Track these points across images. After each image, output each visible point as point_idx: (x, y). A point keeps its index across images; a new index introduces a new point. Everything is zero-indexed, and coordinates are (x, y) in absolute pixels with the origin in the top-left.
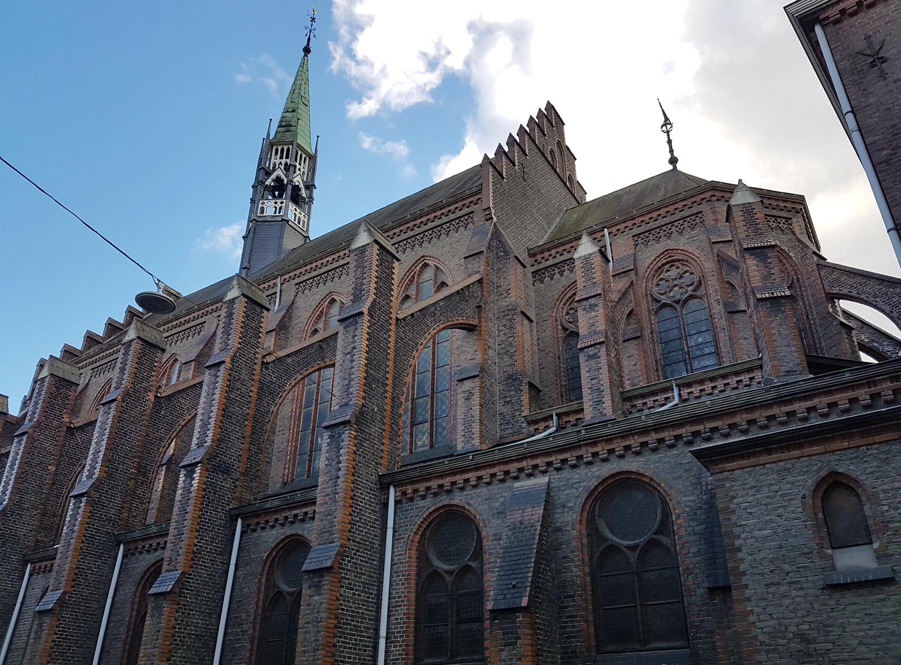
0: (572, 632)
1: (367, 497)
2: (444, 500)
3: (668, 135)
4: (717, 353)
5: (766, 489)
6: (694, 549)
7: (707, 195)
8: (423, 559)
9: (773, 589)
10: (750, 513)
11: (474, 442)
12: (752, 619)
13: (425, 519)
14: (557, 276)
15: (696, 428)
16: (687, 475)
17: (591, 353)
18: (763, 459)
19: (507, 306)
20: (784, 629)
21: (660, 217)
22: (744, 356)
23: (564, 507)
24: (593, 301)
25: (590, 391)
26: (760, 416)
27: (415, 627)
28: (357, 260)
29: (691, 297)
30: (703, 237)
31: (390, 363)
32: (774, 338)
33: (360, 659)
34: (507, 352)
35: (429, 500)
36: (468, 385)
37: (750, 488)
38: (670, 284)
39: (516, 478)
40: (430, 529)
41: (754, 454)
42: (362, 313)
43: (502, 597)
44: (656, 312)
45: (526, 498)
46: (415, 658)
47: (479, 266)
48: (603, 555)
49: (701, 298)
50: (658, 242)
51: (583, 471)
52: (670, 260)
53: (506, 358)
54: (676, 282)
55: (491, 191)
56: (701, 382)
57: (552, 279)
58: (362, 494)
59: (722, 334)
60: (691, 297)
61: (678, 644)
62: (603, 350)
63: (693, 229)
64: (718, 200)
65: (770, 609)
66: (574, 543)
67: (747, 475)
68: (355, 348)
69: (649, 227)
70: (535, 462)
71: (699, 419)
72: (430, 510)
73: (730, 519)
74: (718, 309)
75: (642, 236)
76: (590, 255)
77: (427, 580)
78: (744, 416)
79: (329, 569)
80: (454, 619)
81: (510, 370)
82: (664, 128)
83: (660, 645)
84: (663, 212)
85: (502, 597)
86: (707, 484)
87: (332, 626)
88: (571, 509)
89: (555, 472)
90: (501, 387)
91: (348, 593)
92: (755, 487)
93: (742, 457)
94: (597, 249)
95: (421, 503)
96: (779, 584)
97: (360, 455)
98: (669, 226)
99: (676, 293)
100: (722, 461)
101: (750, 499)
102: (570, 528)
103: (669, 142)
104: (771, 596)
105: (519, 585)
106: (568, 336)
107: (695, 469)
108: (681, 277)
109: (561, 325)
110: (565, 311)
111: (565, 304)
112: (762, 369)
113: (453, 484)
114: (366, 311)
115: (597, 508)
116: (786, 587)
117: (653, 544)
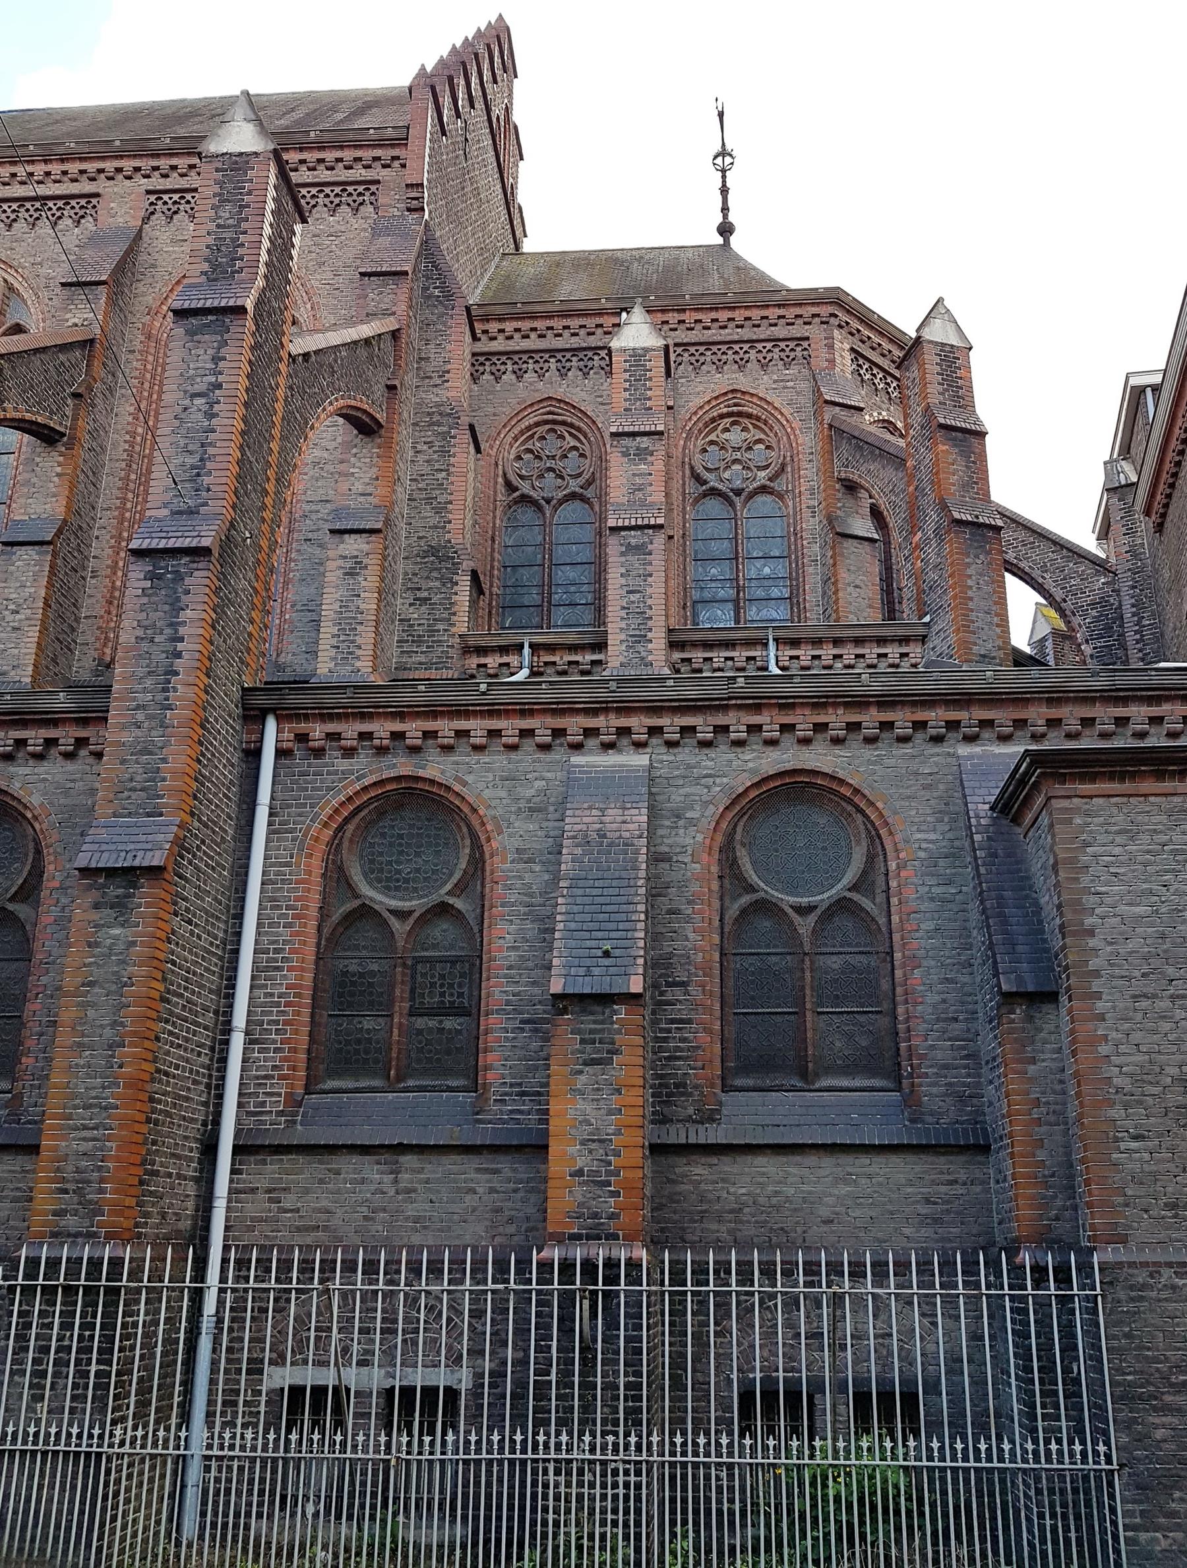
0: (678, 1049)
1: (227, 731)
2: (402, 765)
3: (724, 177)
4: (794, 600)
5: (1146, 838)
6: (928, 925)
7: (824, 311)
8: (336, 878)
9: (1144, 1004)
10: (1116, 875)
11: (358, 664)
12: (1104, 1049)
13: (350, 799)
14: (509, 377)
15: (953, 715)
16: (927, 794)
17: (633, 542)
18: (1147, 786)
19: (438, 405)
20: (1158, 1070)
21: (731, 325)
22: (851, 616)
23: (678, 817)
24: (645, 442)
25: (623, 613)
26: (1071, 714)
27: (312, 1015)
28: (220, 183)
29: (763, 490)
30: (805, 386)
31: (274, 446)
32: (970, 593)
33: (191, 1071)
34: (429, 500)
35: (362, 761)
36: (353, 545)
37: (1119, 832)
38: (730, 455)
39: (577, 747)
40: (357, 820)
41: (1133, 776)
42: (241, 310)
43: (582, 971)
44: (696, 501)
45: (609, 788)
46: (308, 1077)
47: (396, 304)
48: (750, 916)
49: (781, 496)
50: (719, 370)
51: (722, 755)
52: (736, 411)
53: (427, 512)
54: (738, 455)
55: (427, 150)
56: (817, 642)
57: (498, 379)
58: (217, 721)
59: (811, 570)
60: (763, 490)
61: (877, 1082)
62: (659, 540)
63: (787, 366)
64: (840, 326)
65: (1137, 1037)
66: (695, 887)
67: (1115, 811)
68: (219, 386)
69: (708, 335)
70: (623, 722)
71: (964, 700)
72: (366, 782)
73: (1078, 879)
74: (812, 525)
75: (692, 349)
76: (646, 350)
77: (347, 924)
78: (1044, 710)
79: (154, 872)
80: (407, 1005)
81: (434, 539)
82: (719, 160)
83: (845, 1083)
84: (739, 315)
85: (582, 971)
86: (977, 817)
87: (157, 995)
88: (692, 823)
89: (664, 750)
90: (411, 568)
91: (184, 930)
92: (1127, 831)
93: (1112, 777)
94: (661, 343)
95: (343, 764)
96: (1155, 996)
97: (219, 634)
98: (746, 347)
99: (734, 476)
100: (1074, 777)
101: (1117, 851)
102: (687, 859)
103: (724, 191)
104: (1139, 1015)
105: (617, 952)
106: (516, 502)
107: (941, 787)
108: (750, 448)
109: (505, 474)
110: (513, 451)
111: (516, 439)
112: (923, 644)
113: (50, 743)
114: (249, 305)
115: (739, 829)
116: (1166, 1003)
117: (842, 906)
